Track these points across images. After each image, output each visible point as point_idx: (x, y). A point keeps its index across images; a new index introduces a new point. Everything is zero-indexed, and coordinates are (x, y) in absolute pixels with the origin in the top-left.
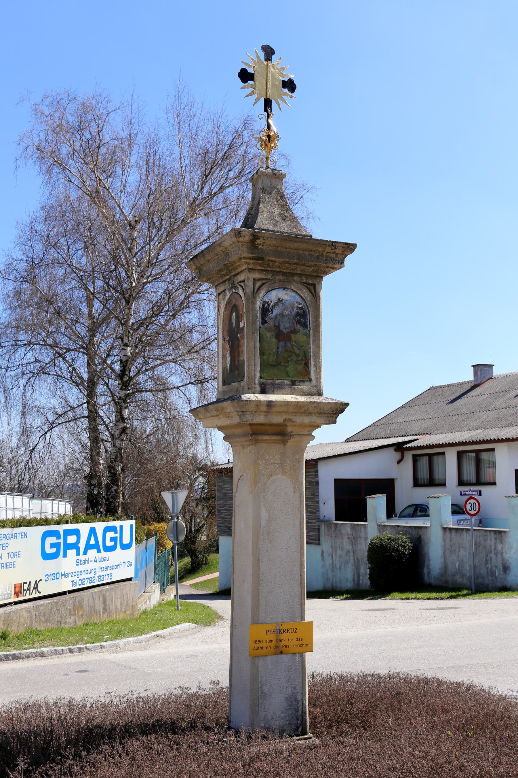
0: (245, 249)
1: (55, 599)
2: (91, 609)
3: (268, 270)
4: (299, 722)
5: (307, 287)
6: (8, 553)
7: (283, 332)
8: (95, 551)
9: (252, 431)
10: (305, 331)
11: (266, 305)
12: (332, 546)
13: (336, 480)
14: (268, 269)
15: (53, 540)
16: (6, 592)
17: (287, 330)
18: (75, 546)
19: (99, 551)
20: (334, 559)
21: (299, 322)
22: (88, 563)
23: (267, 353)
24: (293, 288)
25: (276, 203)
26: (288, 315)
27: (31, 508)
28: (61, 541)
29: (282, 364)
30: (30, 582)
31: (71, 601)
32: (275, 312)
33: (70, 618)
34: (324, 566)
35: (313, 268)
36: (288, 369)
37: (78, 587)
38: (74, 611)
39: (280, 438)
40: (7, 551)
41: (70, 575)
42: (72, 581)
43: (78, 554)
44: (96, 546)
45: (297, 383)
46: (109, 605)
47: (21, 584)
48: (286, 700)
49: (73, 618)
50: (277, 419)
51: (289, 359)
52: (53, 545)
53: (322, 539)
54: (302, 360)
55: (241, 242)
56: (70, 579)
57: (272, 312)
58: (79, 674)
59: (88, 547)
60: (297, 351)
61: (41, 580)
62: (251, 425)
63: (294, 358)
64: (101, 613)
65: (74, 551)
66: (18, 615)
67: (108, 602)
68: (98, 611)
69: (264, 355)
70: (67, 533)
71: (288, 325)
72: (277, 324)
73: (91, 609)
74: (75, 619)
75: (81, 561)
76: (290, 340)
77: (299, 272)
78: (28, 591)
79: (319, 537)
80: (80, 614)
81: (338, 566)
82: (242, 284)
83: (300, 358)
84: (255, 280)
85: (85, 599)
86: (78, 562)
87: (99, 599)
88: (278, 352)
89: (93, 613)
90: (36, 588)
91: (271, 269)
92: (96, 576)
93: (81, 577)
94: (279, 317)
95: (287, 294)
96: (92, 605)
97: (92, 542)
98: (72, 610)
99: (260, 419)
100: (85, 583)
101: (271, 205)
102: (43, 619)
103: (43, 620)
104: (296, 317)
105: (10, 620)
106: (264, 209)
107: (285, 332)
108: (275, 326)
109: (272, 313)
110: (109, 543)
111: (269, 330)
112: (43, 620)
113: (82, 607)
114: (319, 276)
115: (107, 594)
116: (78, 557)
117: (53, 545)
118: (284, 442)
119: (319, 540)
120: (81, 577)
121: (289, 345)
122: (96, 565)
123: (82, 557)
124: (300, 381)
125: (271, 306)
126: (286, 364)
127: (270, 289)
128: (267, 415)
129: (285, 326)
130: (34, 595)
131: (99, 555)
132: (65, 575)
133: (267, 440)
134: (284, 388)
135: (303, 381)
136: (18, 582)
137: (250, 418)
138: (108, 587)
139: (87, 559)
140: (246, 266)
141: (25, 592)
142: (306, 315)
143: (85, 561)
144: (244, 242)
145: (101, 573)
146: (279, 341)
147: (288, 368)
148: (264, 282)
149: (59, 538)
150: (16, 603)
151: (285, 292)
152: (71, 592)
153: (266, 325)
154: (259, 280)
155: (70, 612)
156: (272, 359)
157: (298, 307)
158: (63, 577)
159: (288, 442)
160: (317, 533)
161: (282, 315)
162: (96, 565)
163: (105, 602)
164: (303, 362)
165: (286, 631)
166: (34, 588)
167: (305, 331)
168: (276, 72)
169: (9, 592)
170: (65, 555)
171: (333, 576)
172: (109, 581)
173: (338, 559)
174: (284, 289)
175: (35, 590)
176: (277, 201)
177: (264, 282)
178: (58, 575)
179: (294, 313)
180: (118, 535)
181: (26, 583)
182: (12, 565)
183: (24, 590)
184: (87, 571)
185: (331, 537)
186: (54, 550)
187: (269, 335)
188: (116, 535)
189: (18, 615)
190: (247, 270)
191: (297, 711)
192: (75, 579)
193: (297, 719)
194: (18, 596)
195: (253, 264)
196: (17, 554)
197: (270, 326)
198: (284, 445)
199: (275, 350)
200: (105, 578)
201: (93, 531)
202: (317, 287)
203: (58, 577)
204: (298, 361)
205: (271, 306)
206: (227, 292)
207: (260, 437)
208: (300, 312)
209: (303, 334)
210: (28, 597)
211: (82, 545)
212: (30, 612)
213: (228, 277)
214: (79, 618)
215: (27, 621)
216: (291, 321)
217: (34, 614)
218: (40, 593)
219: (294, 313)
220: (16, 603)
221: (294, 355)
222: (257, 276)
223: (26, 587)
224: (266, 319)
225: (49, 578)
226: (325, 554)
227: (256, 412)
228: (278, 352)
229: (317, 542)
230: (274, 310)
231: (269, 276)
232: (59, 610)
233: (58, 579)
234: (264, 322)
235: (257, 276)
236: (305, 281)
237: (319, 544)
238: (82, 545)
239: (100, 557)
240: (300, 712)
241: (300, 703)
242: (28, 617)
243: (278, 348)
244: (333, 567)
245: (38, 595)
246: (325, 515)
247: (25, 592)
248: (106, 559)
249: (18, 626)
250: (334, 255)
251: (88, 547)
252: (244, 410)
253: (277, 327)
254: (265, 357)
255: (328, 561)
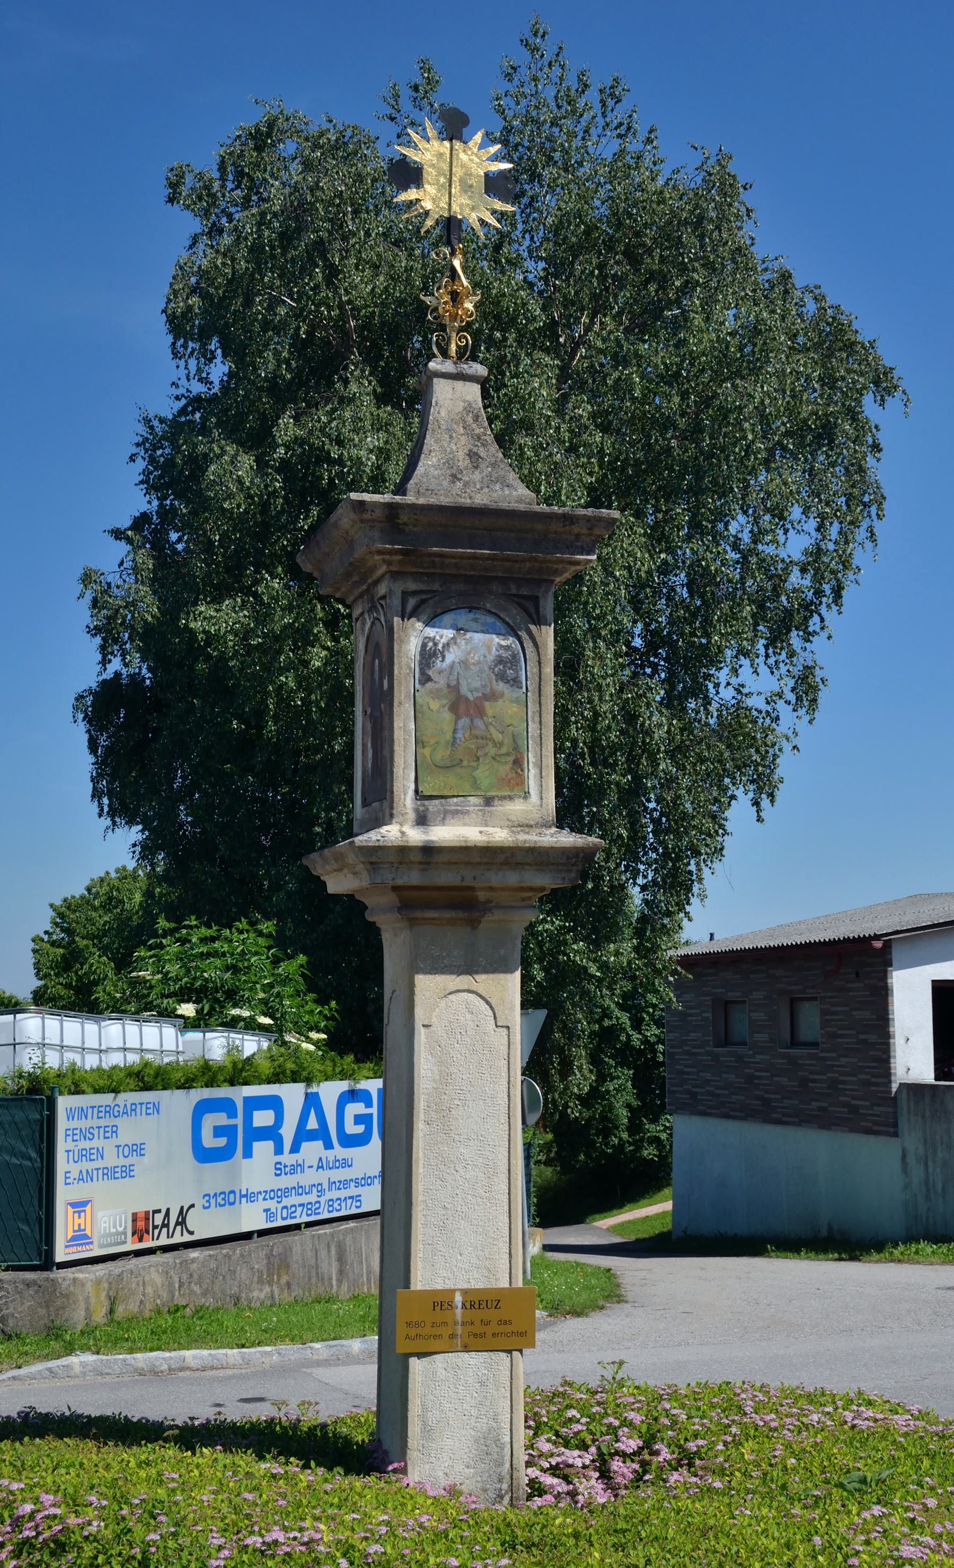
0: (376, 534)
1: (225, 1249)
2: (309, 1272)
3: (434, 574)
4: (505, 1486)
5: (520, 605)
6: (118, 1147)
7: (467, 699)
8: (319, 1144)
9: (401, 901)
10: (515, 695)
11: (430, 644)
12: (925, 1140)
13: (933, 981)
14: (432, 571)
15: (222, 1119)
16: (113, 1230)
17: (476, 694)
18: (271, 1133)
19: (328, 1145)
20: (931, 1170)
21: (501, 677)
22: (303, 1171)
23: (432, 741)
24: (488, 606)
25: (462, 431)
26: (479, 662)
27: (180, 1049)
28: (239, 1121)
29: (465, 763)
30: (168, 1210)
31: (262, 1254)
32: (450, 657)
33: (261, 1290)
34: (907, 1186)
35: (528, 565)
36: (477, 773)
37: (280, 1223)
38: (270, 1275)
39: (461, 914)
40: (115, 1141)
41: (261, 1197)
42: (266, 1211)
43: (279, 1150)
44: (322, 1134)
45: (496, 802)
46: (352, 1264)
47: (147, 1213)
48: (476, 1441)
49: (267, 1289)
50: (446, 878)
51: (479, 753)
52: (219, 1131)
53: (903, 1124)
54: (508, 754)
55: (368, 521)
56: (261, 1205)
57: (444, 657)
58: (247, 1406)
59: (302, 1136)
60: (497, 736)
61: (193, 1206)
62: (395, 889)
63: (493, 751)
64: (334, 1282)
65: (269, 1145)
66: (140, 1279)
67: (350, 1257)
68: (326, 1277)
69: (424, 747)
70: (253, 1104)
71: (477, 684)
72: (454, 683)
73: (309, 1272)
74: (272, 1292)
75: (285, 1166)
76: (481, 713)
77: (500, 574)
78: (165, 1230)
79: (896, 1118)
80: (284, 1280)
81: (939, 1186)
82: (383, 602)
83: (504, 750)
84: (405, 595)
85: (294, 1249)
86: (279, 1169)
87: (329, 1251)
88: (454, 738)
89: (314, 1280)
90: (182, 1222)
91: (439, 571)
92: (323, 1200)
93: (287, 1202)
94: (457, 668)
95: (476, 620)
96: (313, 1262)
97: (312, 1124)
98: (265, 1272)
99: (413, 878)
100: (298, 1214)
101: (451, 437)
102: (197, 1289)
103: (199, 1292)
104: (496, 666)
105: (123, 1289)
106: (435, 447)
107: (471, 699)
108: (449, 686)
109: (443, 661)
110: (352, 1128)
111: (436, 694)
112: (199, 1292)
113: (288, 1266)
114: (545, 581)
115: (348, 1240)
116: (279, 1158)
117: (219, 1131)
118: (473, 924)
119: (895, 1125)
120: (287, 1202)
121: (479, 723)
122: (323, 1177)
123: (287, 1158)
124: (503, 798)
125: (440, 647)
126: (475, 764)
127: (439, 611)
128: (426, 870)
129: (471, 686)
130: (177, 1239)
131: (330, 1155)
132: (250, 1197)
133: (434, 919)
134: (468, 812)
135: (511, 798)
136: (141, 1208)
137: (390, 876)
138: (352, 1224)
139: (300, 1162)
140: (384, 568)
141: (156, 1232)
142: (519, 661)
143: (297, 1168)
144: (373, 521)
145: (334, 1194)
146: (458, 718)
147: (477, 772)
148: (424, 597)
149: (232, 1114)
150: (138, 1253)
151: (471, 616)
152: (262, 1233)
153: (429, 685)
154: (415, 593)
155: (260, 1277)
156: (442, 754)
157: (502, 646)
158: (244, 1200)
159: (480, 922)
160: (890, 1110)
161: (464, 663)
162: (323, 1177)
163: (341, 1258)
164: (512, 759)
165: (477, 1306)
166: (177, 1224)
167: (515, 695)
168: (471, 160)
169: (121, 1229)
170: (248, 1153)
171: (929, 1209)
172: (354, 1211)
173: (938, 1170)
174: (471, 609)
175: (179, 1228)
176: (464, 428)
177: (424, 597)
178: (232, 1196)
179: (492, 658)
180: (374, 1110)
181: (159, 1211)
182: (127, 1172)
183: (155, 1227)
184: (299, 1190)
185: (923, 1117)
186: (222, 1142)
187: (435, 705)
188: (368, 1111)
189: (140, 1279)
190: (387, 576)
191: (501, 1465)
192: (272, 1205)
193: (500, 1481)
194: (141, 1240)
195: (399, 562)
196: (138, 1149)
197: (437, 686)
198: (474, 928)
199: (449, 736)
200: (343, 1204)
201: (312, 1101)
202: (541, 602)
203: (232, 1200)
204: (500, 755)
205: (440, 647)
206: (366, 616)
207: (419, 914)
208: (505, 654)
209: (512, 702)
210: (164, 1241)
211: (288, 1132)
212: (167, 1273)
213: (364, 587)
214: (282, 1290)
215: (161, 1293)
216: (484, 676)
217: (177, 1280)
218: (191, 1233)
219: (490, 659)
220: (138, 1253)
221: (491, 745)
222: (412, 586)
223: (159, 1219)
224: (430, 673)
225: (213, 1201)
226: (911, 1159)
227: (400, 863)
228: (454, 738)
229: (891, 1130)
230: (446, 653)
231: (436, 586)
232: (235, 1272)
233: (233, 1204)
234: (425, 679)
235: (412, 586)
236: (514, 591)
237: (896, 1135)
238: (288, 1132)
239: (331, 1159)
240: (508, 1465)
241: (507, 1450)
242: (163, 1285)
243: (455, 731)
244: (928, 1190)
245: (187, 1238)
246: (911, 1066)
247: (156, 1232)
248: (346, 1164)
249: (141, 1302)
250: (573, 538)
251: (302, 1136)
252: (374, 859)
253: (454, 689)
254: (427, 752)
255: (917, 1173)
